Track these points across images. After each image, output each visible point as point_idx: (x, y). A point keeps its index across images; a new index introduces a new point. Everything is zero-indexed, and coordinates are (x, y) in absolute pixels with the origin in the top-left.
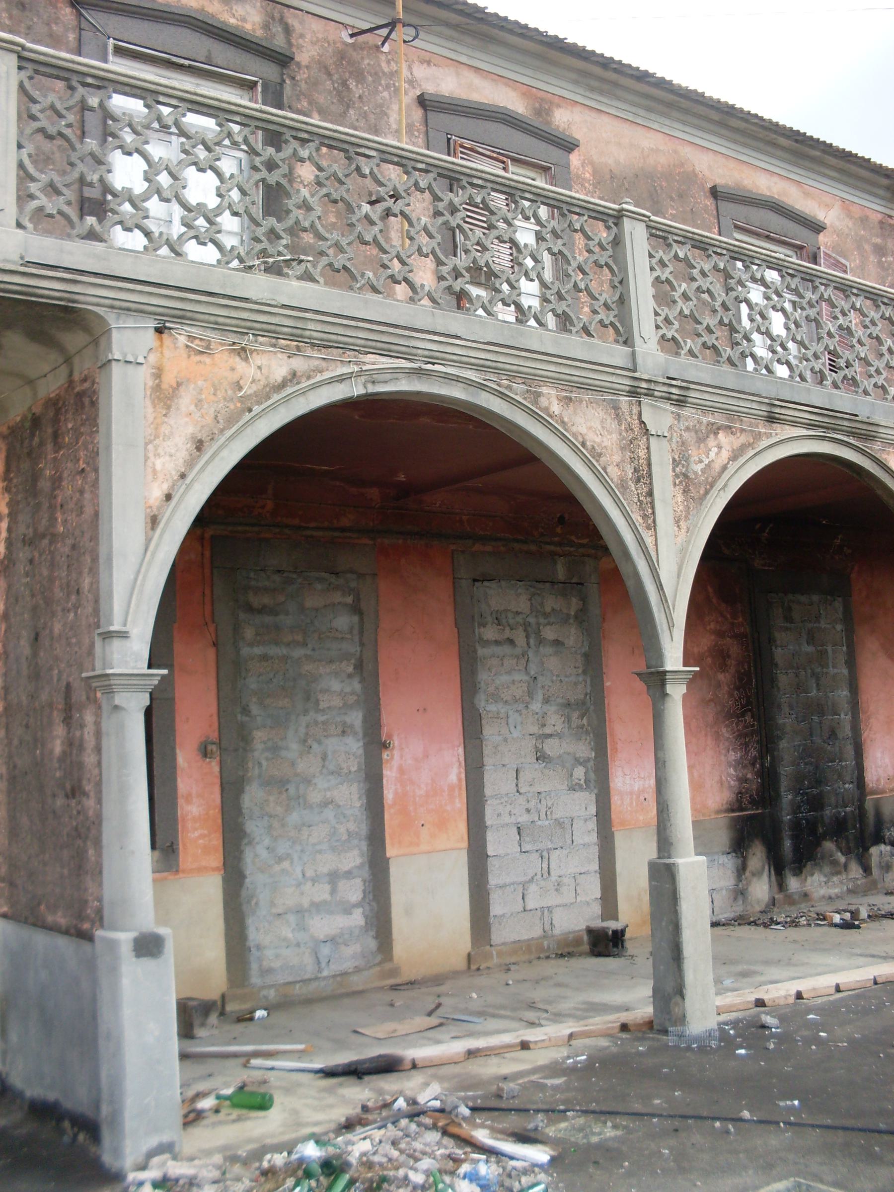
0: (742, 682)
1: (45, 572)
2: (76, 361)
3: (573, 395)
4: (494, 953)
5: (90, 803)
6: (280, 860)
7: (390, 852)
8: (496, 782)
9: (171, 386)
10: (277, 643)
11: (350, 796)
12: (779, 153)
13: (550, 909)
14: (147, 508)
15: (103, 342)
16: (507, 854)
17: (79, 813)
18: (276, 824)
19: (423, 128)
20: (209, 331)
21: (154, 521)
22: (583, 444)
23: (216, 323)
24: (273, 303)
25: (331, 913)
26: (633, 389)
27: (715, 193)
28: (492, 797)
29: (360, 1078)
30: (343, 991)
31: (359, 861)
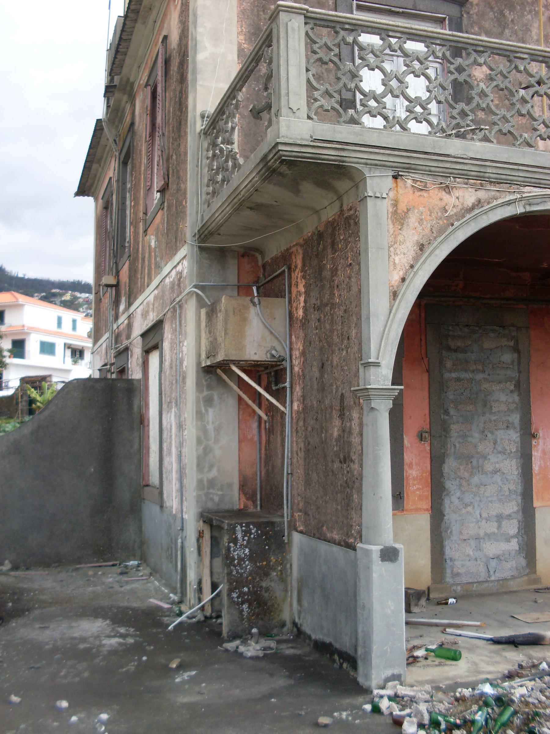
1: (328, 327)
2: (345, 198)
5: (356, 466)
6: (466, 505)
7: (536, 504)
9: (404, 211)
10: (466, 370)
11: (511, 467)
14: (390, 287)
15: (361, 185)
17: (348, 472)
18: (464, 483)
20: (425, 176)
21: (395, 295)
23: (430, 171)
24: (465, 157)
25: (497, 540)
29: (516, 647)
31: (516, 509)
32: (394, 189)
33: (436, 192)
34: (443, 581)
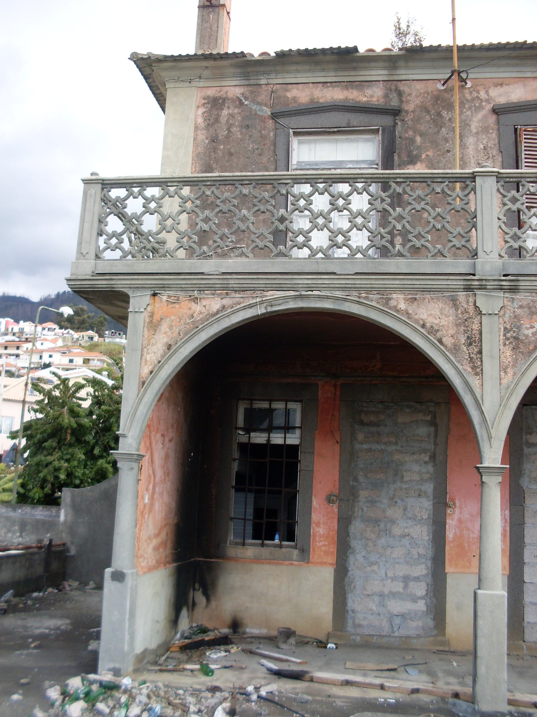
3: (417, 296)
6: (371, 564)
9: (158, 321)
10: (378, 443)
11: (422, 533)
18: (370, 544)
19: (496, 127)
20: (179, 292)
22: (423, 326)
23: (182, 288)
26: (467, 287)
28: (530, 544)
30: (406, 647)
31: (424, 572)
32: (152, 304)
33: (187, 304)
34: (344, 630)
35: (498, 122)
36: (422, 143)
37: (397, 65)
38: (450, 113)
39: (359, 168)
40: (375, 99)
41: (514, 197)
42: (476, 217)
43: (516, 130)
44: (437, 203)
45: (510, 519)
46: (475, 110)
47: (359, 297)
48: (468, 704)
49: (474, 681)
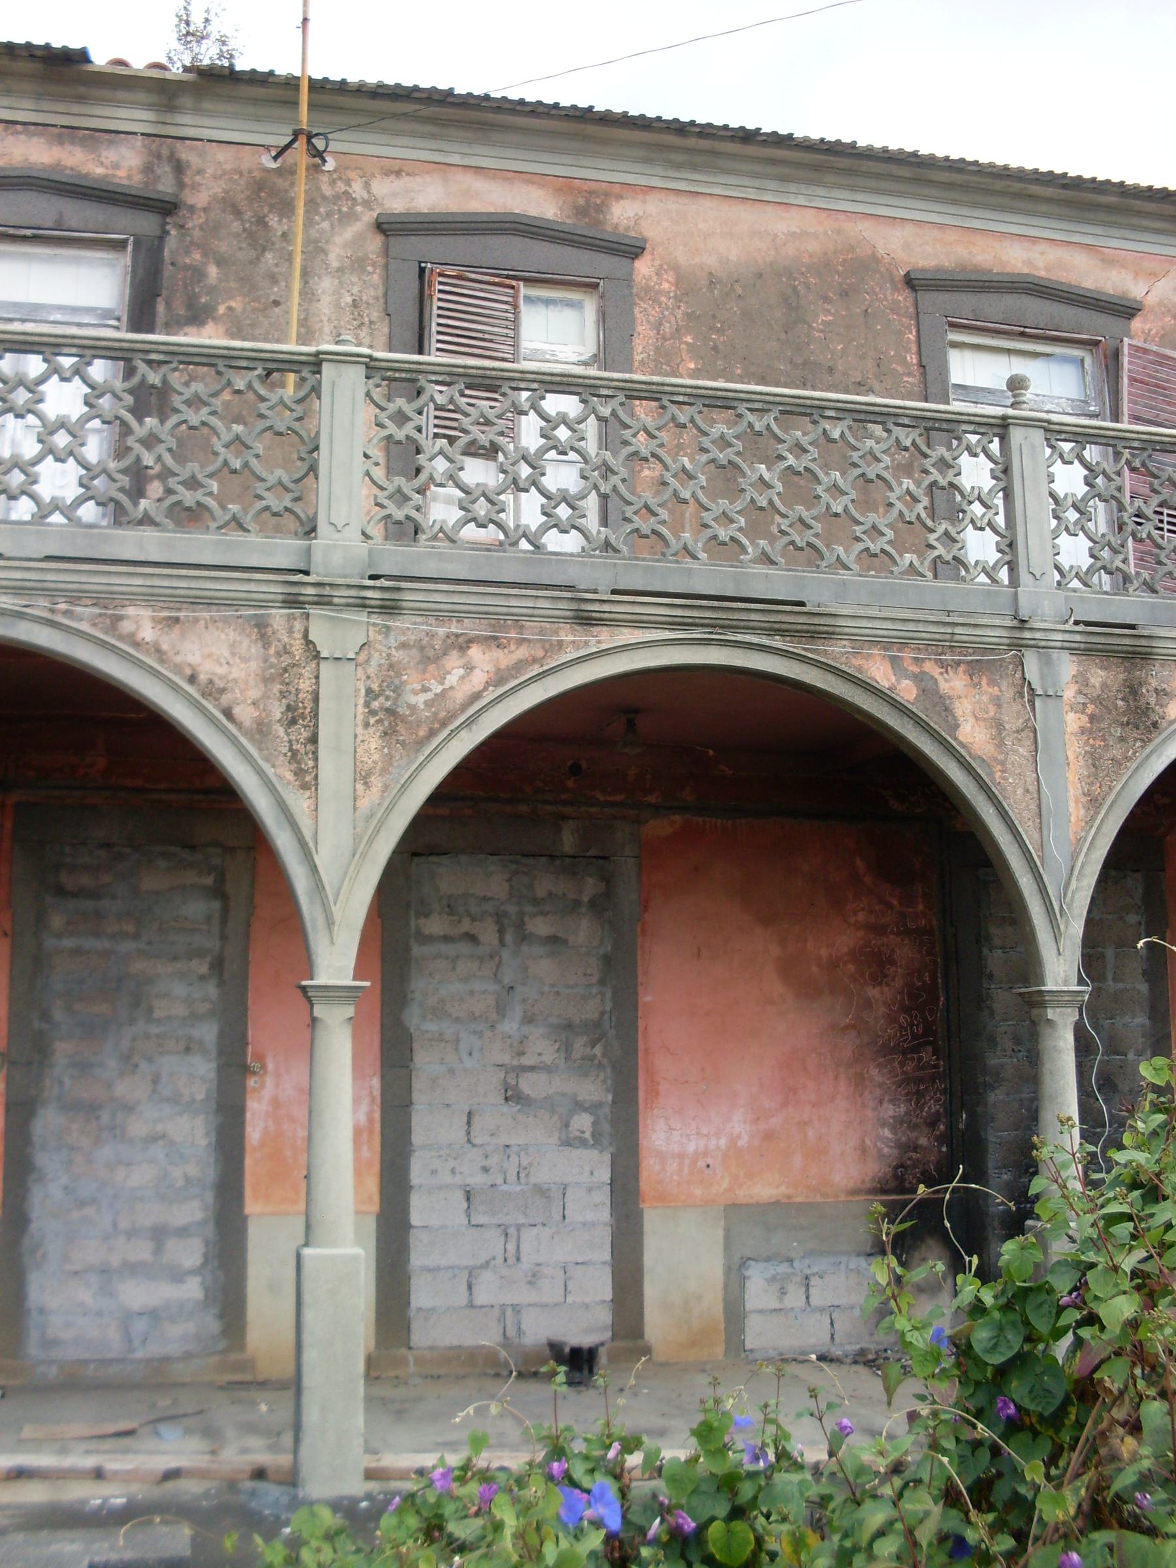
0: (917, 1000)
3: (182, 614)
4: (411, 1359)
6: (82, 1204)
7: (251, 1207)
8: (431, 1128)
10: (96, 934)
11: (194, 1133)
12: (1043, 208)
13: (517, 1309)
16: (443, 1227)
19: (381, 261)
22: (192, 679)
26: (291, 598)
27: (911, 282)
31: (199, 1215)
35: (386, 251)
36: (220, 280)
37: (177, 102)
38: (284, 220)
39: (79, 325)
40: (122, 173)
41: (722, 436)
42: (317, 448)
43: (422, 271)
44: (244, 413)
45: (382, 1095)
46: (339, 220)
47: (52, 611)
48: (283, 1488)
49: (297, 1440)
